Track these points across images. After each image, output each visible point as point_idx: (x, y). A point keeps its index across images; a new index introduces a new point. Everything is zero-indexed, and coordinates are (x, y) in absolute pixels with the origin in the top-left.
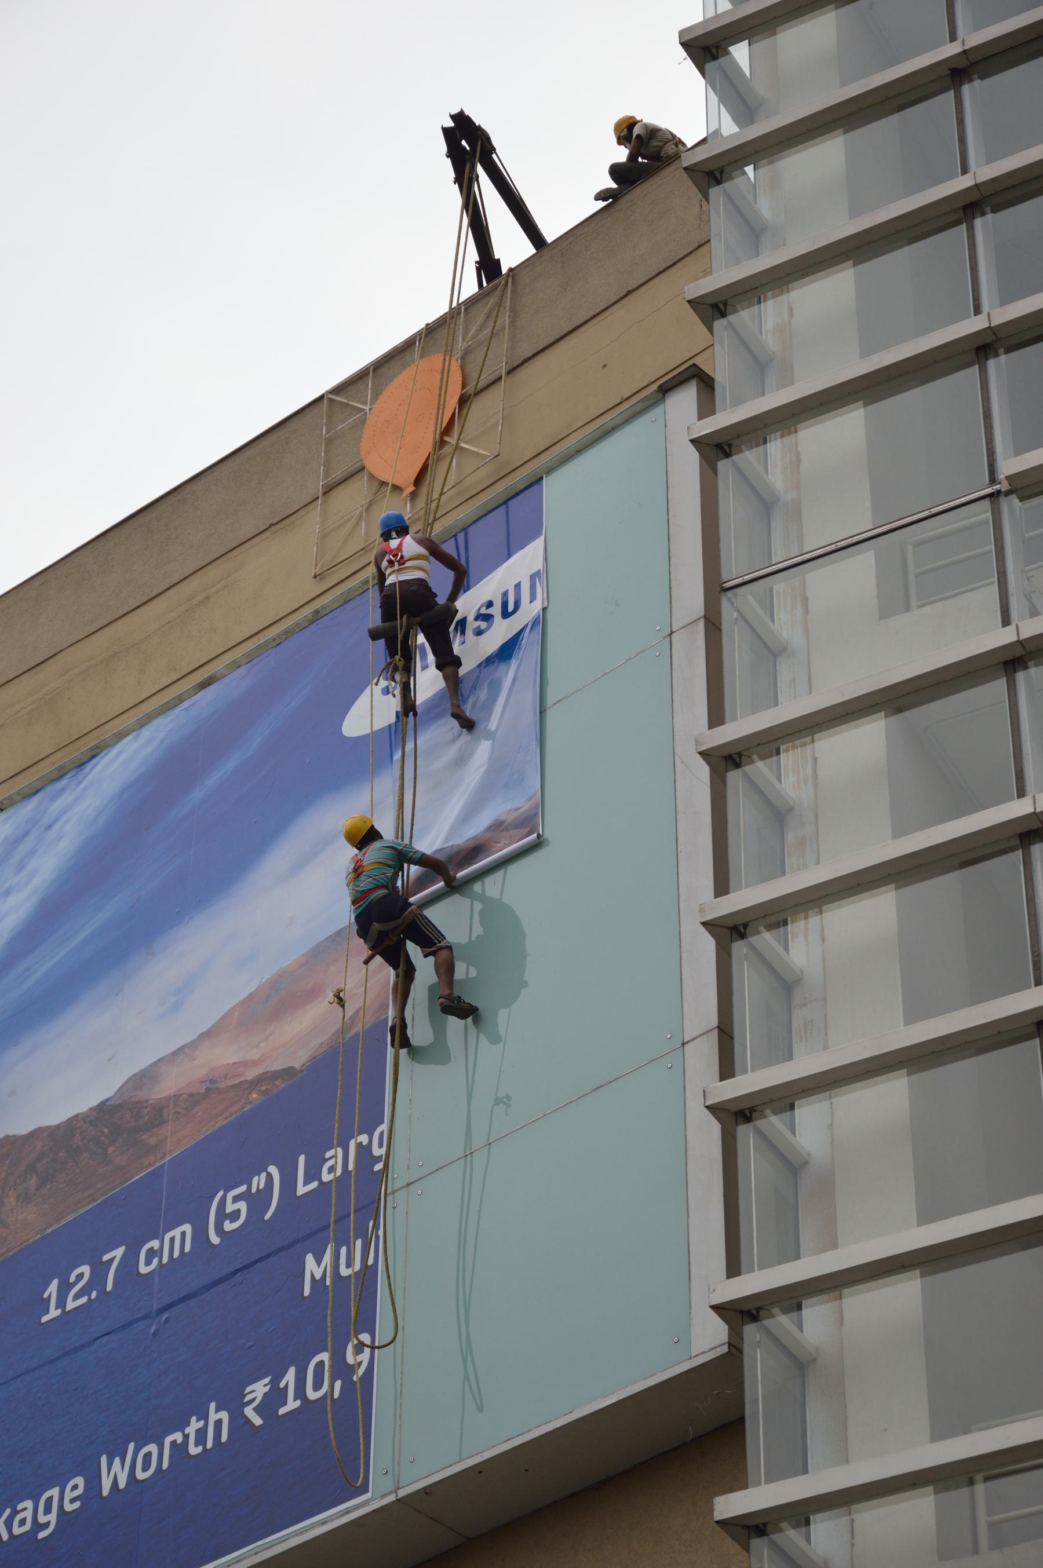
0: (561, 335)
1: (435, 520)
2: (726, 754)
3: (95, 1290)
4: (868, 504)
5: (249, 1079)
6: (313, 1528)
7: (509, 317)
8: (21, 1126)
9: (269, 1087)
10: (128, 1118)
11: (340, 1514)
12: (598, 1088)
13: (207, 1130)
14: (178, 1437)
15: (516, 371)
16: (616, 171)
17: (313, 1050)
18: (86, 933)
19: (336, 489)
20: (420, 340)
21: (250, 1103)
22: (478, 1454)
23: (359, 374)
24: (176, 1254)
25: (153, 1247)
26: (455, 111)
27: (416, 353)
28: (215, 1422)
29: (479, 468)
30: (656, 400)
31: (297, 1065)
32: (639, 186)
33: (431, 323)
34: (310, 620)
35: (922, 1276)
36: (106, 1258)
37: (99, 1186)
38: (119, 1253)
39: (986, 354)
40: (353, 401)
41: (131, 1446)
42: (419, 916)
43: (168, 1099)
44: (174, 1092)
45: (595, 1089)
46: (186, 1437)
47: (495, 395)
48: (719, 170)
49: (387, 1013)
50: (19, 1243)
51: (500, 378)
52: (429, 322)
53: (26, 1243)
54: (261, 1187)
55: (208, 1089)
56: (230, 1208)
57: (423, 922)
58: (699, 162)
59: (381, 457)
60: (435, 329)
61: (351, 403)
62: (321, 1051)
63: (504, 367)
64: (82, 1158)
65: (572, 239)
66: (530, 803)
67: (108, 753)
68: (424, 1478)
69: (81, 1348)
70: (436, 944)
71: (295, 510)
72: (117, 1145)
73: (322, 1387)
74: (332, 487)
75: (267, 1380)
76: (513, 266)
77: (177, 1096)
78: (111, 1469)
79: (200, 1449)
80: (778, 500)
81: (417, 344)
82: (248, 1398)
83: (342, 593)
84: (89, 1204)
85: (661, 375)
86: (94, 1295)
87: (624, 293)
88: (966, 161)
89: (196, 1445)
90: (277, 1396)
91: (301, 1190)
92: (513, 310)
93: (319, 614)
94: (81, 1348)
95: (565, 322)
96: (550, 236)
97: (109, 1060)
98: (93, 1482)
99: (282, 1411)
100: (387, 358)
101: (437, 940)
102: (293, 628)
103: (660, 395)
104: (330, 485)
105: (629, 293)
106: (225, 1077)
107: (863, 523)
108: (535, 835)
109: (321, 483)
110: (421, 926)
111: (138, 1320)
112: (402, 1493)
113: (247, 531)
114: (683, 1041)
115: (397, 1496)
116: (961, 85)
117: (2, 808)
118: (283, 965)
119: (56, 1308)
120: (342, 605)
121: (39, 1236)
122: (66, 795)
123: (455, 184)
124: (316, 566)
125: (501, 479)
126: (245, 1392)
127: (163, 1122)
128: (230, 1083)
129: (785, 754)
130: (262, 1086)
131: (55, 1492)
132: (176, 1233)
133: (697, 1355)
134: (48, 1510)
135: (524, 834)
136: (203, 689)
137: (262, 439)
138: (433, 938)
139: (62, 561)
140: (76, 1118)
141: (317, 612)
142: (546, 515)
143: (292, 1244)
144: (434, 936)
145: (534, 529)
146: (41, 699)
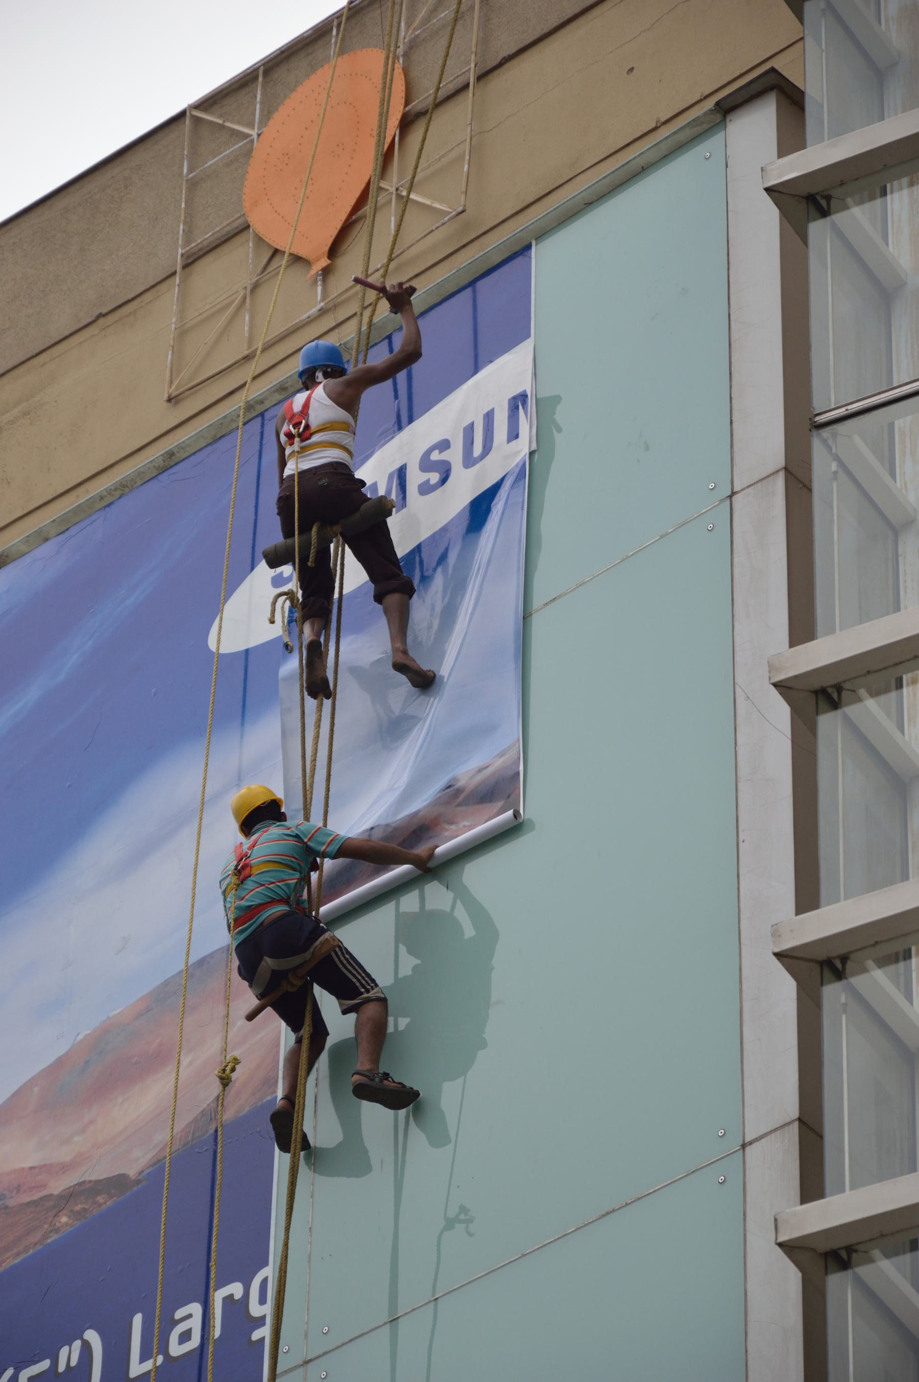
5: (56, 1193)
9: (86, 1207)
12: (607, 1214)
14: (236, 1289)
15: (491, 76)
21: (57, 1231)
29: (432, 231)
30: (712, 124)
34: (159, 467)
40: (232, 122)
42: (337, 949)
45: (604, 1216)
51: (466, 86)
54: (74, 1362)
57: (342, 959)
60: (362, 9)
61: (228, 124)
66: (502, 759)
70: (362, 993)
71: (138, 292)
74: (195, 257)
81: (334, 32)
91: (136, 1368)
93: (173, 458)
100: (284, 55)
103: (718, 117)
104: (195, 253)
106: (18, 1188)
109: (180, 251)
110: (340, 966)
113: (63, 323)
114: (744, 1141)
118: (111, 1015)
124: (171, 382)
128: (25, 1198)
129: (911, 688)
130: (77, 1205)
138: (358, 984)
141: (171, 454)
144: (359, 981)
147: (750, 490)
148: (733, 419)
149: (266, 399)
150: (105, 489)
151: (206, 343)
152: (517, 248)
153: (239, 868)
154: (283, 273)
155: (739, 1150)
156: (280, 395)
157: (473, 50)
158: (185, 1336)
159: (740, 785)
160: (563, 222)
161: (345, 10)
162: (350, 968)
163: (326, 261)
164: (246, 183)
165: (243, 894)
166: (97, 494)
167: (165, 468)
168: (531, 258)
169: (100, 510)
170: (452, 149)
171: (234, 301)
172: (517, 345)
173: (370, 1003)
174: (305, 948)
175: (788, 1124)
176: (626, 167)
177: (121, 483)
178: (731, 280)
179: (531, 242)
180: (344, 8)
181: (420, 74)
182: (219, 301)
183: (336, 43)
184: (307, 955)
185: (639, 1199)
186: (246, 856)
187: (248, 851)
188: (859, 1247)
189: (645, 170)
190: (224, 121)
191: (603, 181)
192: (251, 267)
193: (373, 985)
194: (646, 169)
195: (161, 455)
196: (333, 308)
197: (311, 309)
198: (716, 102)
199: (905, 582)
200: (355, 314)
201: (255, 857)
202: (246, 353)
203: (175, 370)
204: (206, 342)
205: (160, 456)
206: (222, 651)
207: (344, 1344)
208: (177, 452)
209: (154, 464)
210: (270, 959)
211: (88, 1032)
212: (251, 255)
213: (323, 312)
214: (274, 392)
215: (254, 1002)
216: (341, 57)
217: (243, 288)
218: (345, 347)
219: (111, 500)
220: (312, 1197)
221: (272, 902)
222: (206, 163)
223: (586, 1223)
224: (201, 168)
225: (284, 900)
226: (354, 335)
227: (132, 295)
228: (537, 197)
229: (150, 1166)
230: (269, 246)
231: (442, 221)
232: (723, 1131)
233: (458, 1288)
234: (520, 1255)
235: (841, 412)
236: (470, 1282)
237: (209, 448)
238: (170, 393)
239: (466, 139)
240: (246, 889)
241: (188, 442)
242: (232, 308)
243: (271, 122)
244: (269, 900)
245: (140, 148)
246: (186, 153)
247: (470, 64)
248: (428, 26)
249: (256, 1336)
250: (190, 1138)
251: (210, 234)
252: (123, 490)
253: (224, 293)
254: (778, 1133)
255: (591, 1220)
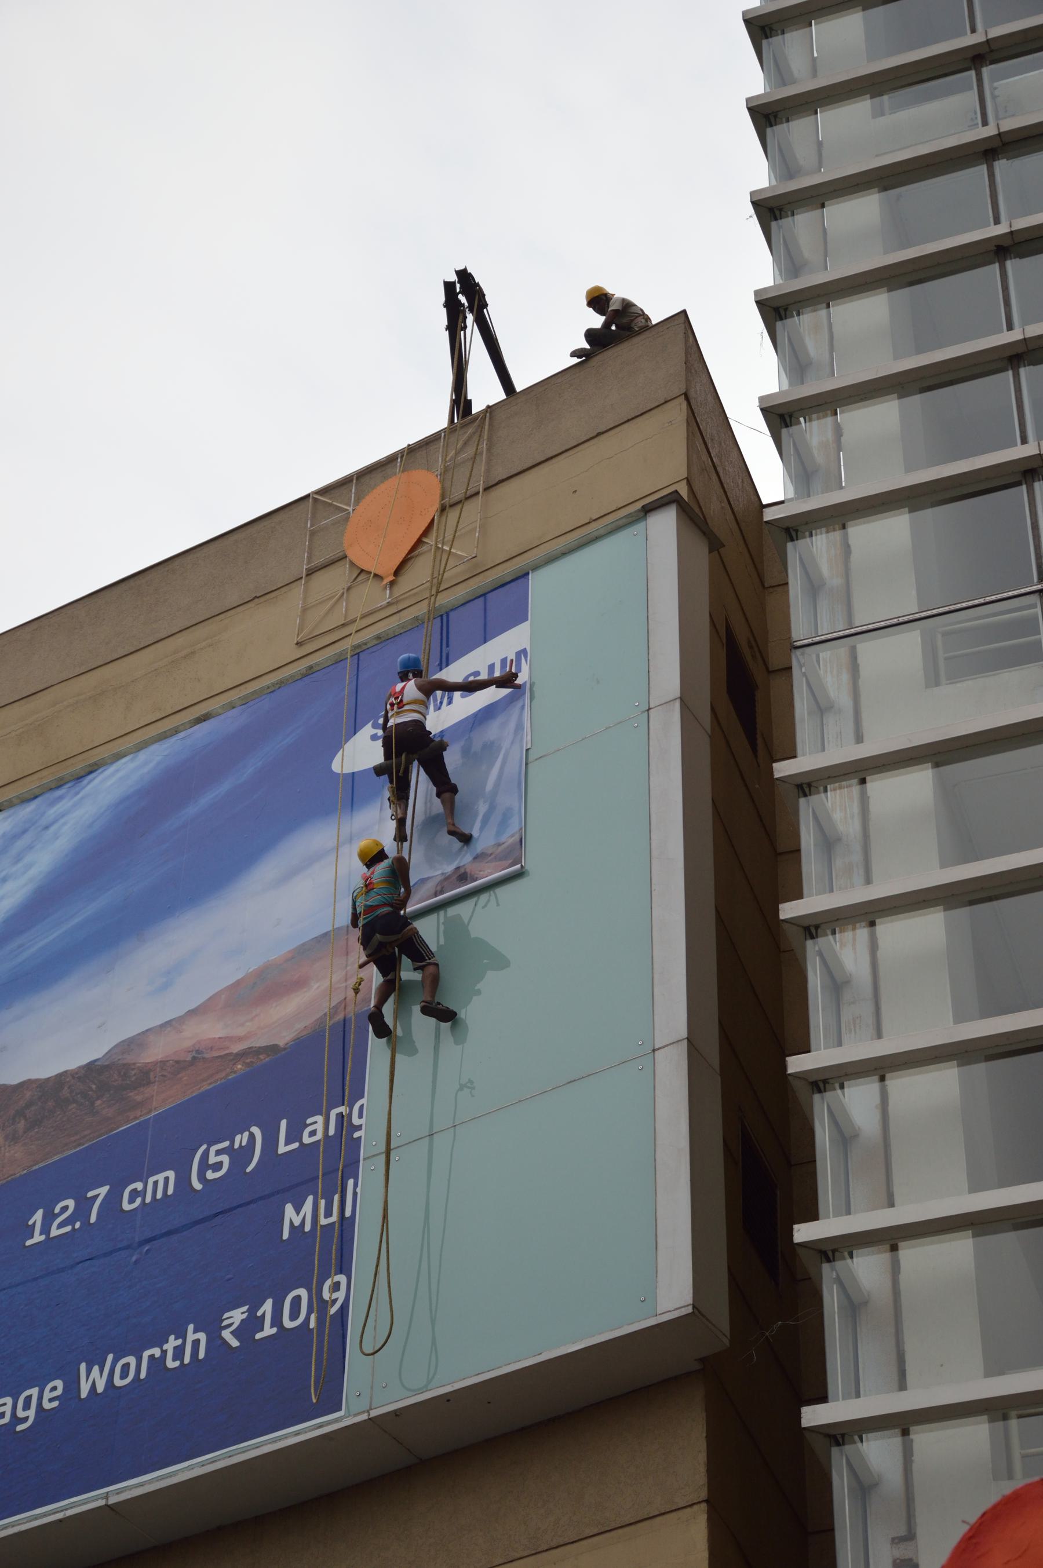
2: (799, 783)
3: (78, 1221)
4: (914, 592)
5: (234, 1052)
6: (286, 1438)
7: (487, 444)
8: (12, 1077)
9: (254, 1061)
10: (116, 1078)
11: (313, 1427)
13: (192, 1092)
14: (156, 1352)
15: (491, 489)
16: (591, 335)
17: (297, 1032)
18: (77, 920)
19: (317, 572)
21: (235, 1072)
22: (449, 1384)
23: (342, 481)
24: (159, 1196)
25: (136, 1189)
26: (460, 268)
27: (398, 467)
28: (193, 1341)
29: (457, 566)
31: (281, 1043)
32: (610, 350)
33: (413, 444)
35: (974, 1236)
36: (90, 1194)
37: (86, 1133)
38: (103, 1191)
39: (1033, 478)
40: (337, 502)
41: (110, 1357)
43: (156, 1063)
44: (161, 1058)
45: (569, 1083)
46: (164, 1353)
47: (472, 510)
48: (784, 307)
50: (6, 1177)
51: (478, 493)
52: (410, 444)
53: (13, 1177)
54: (244, 1143)
55: (194, 1058)
56: (213, 1159)
58: (770, 298)
59: (363, 550)
60: (415, 449)
61: (334, 503)
63: (481, 485)
64: (70, 1108)
65: (546, 387)
66: (513, 838)
67: (105, 770)
68: (396, 1401)
69: (62, 1270)
71: (279, 587)
72: (105, 1099)
73: (297, 1319)
74: (313, 571)
75: (245, 1308)
76: (490, 405)
77: (163, 1063)
78: (90, 1374)
79: (177, 1364)
80: (825, 584)
81: (399, 460)
82: (225, 1323)
84: (75, 1147)
86: (78, 1225)
87: (595, 434)
88: (1011, 320)
89: (174, 1360)
90: (254, 1322)
91: (282, 1149)
92: (490, 439)
93: (312, 670)
94: (62, 1270)
95: (539, 453)
96: (519, 386)
97: (99, 1027)
98: (72, 1385)
99: (259, 1336)
100: (369, 470)
102: (287, 680)
103: (642, 514)
104: (313, 569)
105: (599, 434)
106: (212, 1048)
107: (910, 607)
108: (519, 866)
109: (305, 567)
111: (120, 1249)
112: (374, 1413)
113: (233, 599)
115: (369, 1415)
116: (1005, 260)
117: (2, 808)
119: (41, 1234)
121: (25, 1172)
122: (64, 801)
123: (446, 330)
124: (298, 635)
126: (223, 1318)
127: (149, 1083)
128: (216, 1054)
129: (833, 793)
130: (247, 1059)
131: (34, 1392)
132: (160, 1177)
133: (663, 1313)
134: (27, 1406)
135: (507, 865)
136: (198, 724)
137: (249, 527)
139: (36, 622)
140: (65, 1074)
141: (311, 667)
143: (272, 1194)
145: (518, 615)
146: (31, 724)
147: (659, 707)
149: (368, 642)
152: (520, 574)
158: (313, 1133)
159: (653, 861)
161: (406, 449)
183: (400, 466)
188: (830, 1081)
197: (383, 602)
199: (829, 738)
200: (427, 598)
206: (343, 772)
207: (410, 1143)
213: (389, 604)
214: (373, 639)
215: (364, 958)
227: (275, 588)
230: (358, 567)
235: (809, 641)
243: (361, 504)
245: (282, 512)
249: (356, 1135)
250: (317, 1027)
254: (675, 1045)
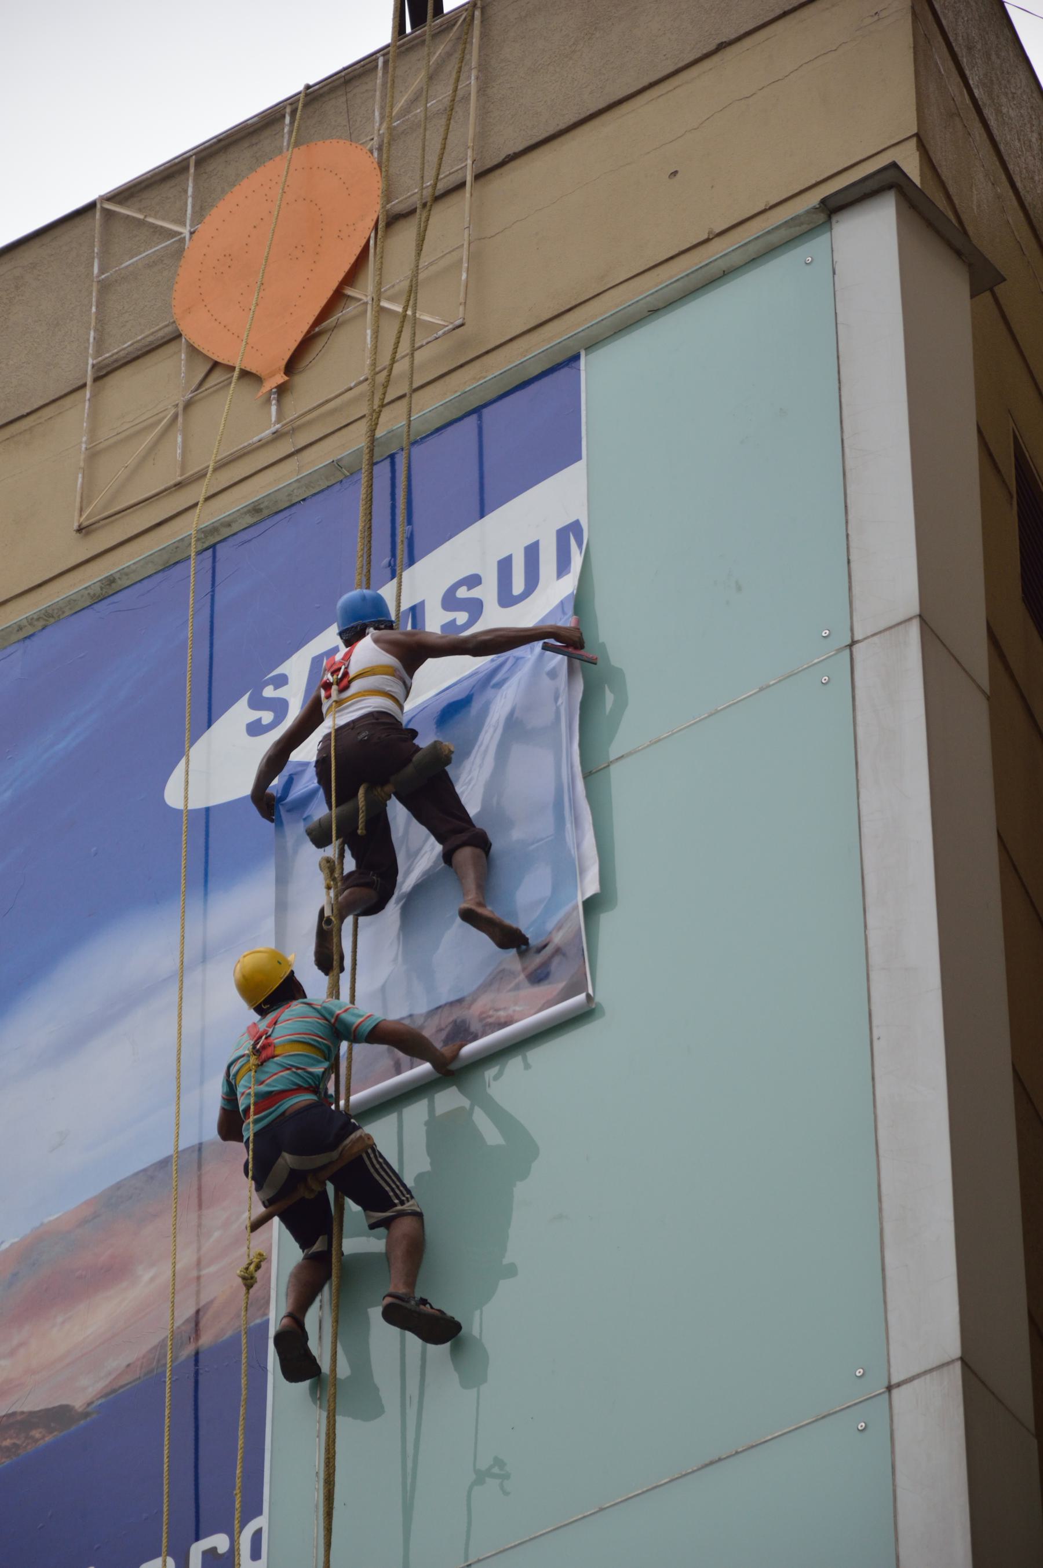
0: (582, 116)
1: (383, 406)
9: (18, 1442)
12: (712, 1463)
14: (220, 1542)
15: (492, 176)
20: (293, 113)
30: (812, 225)
31: (78, 1403)
34: (94, 595)
40: (155, 217)
42: (370, 1151)
49: (266, 1313)
52: (311, 83)
57: (375, 1162)
60: (321, 95)
61: (150, 220)
62: (127, 1378)
63: (469, 167)
70: (395, 1205)
71: (35, 406)
74: (109, 369)
81: (287, 120)
83: (164, 548)
85: (790, 194)
93: (113, 585)
101: (398, 1197)
103: (822, 217)
104: (108, 365)
105: (721, 47)
109: (90, 361)
110: (372, 1170)
114: (889, 1382)
118: (46, 1221)
120: (162, 570)
125: (461, 366)
130: (5, 1439)
138: (391, 1194)
141: (111, 580)
142: (587, 423)
144: (393, 1190)
147: (876, 639)
148: (850, 558)
149: (234, 521)
150: (26, 618)
151: (127, 467)
153: (258, 1047)
154: (234, 387)
155: (883, 1393)
156: (252, 517)
157: (469, 145)
159: (873, 976)
160: (620, 331)
161: (302, 95)
162: (383, 1173)
163: (282, 377)
164: (176, 287)
165: (263, 1077)
166: (15, 623)
167: (102, 597)
168: (579, 370)
169: (19, 641)
170: (443, 256)
171: (160, 421)
172: (545, 479)
173: (405, 1217)
174: (333, 1147)
175: (948, 1364)
176: (704, 270)
177: (46, 612)
178: (843, 400)
179: (579, 352)
180: (300, 93)
181: (399, 171)
182: (137, 422)
183: (291, 132)
184: (335, 1155)
185: (753, 1447)
186: (267, 1034)
187: (267, 1029)
189: (726, 275)
190: (146, 216)
191: (675, 284)
192: (183, 381)
193: (408, 1196)
194: (728, 273)
195: (99, 581)
196: (291, 432)
198: (822, 199)
201: (279, 1035)
202: (179, 479)
203: (86, 499)
204: (126, 465)
205: (97, 582)
206: (189, 808)
208: (119, 578)
209: (89, 591)
210: (290, 1156)
211: (16, 1240)
212: (183, 368)
213: (277, 436)
214: (245, 513)
215: (260, 1210)
216: (297, 148)
217: (174, 406)
218: (339, 465)
219: (30, 630)
220: (318, 1437)
221: (299, 1089)
222: (122, 264)
223: (684, 1473)
224: (117, 268)
225: (311, 1089)
226: (363, 444)
227: (28, 410)
228: (556, 313)
229: (101, 1397)
230: (206, 357)
231: (435, 335)
232: (861, 1371)
233: (515, 1546)
234: (598, 1509)
236: (531, 1539)
237: (160, 575)
238: (81, 521)
239: (463, 245)
240: (267, 1072)
241: (133, 567)
242: (159, 428)
244: (295, 1087)
245: (35, 245)
246: (96, 250)
247: (466, 159)
248: (407, 117)
251: (129, 343)
252: (47, 620)
253: (148, 410)
255: (690, 1470)
